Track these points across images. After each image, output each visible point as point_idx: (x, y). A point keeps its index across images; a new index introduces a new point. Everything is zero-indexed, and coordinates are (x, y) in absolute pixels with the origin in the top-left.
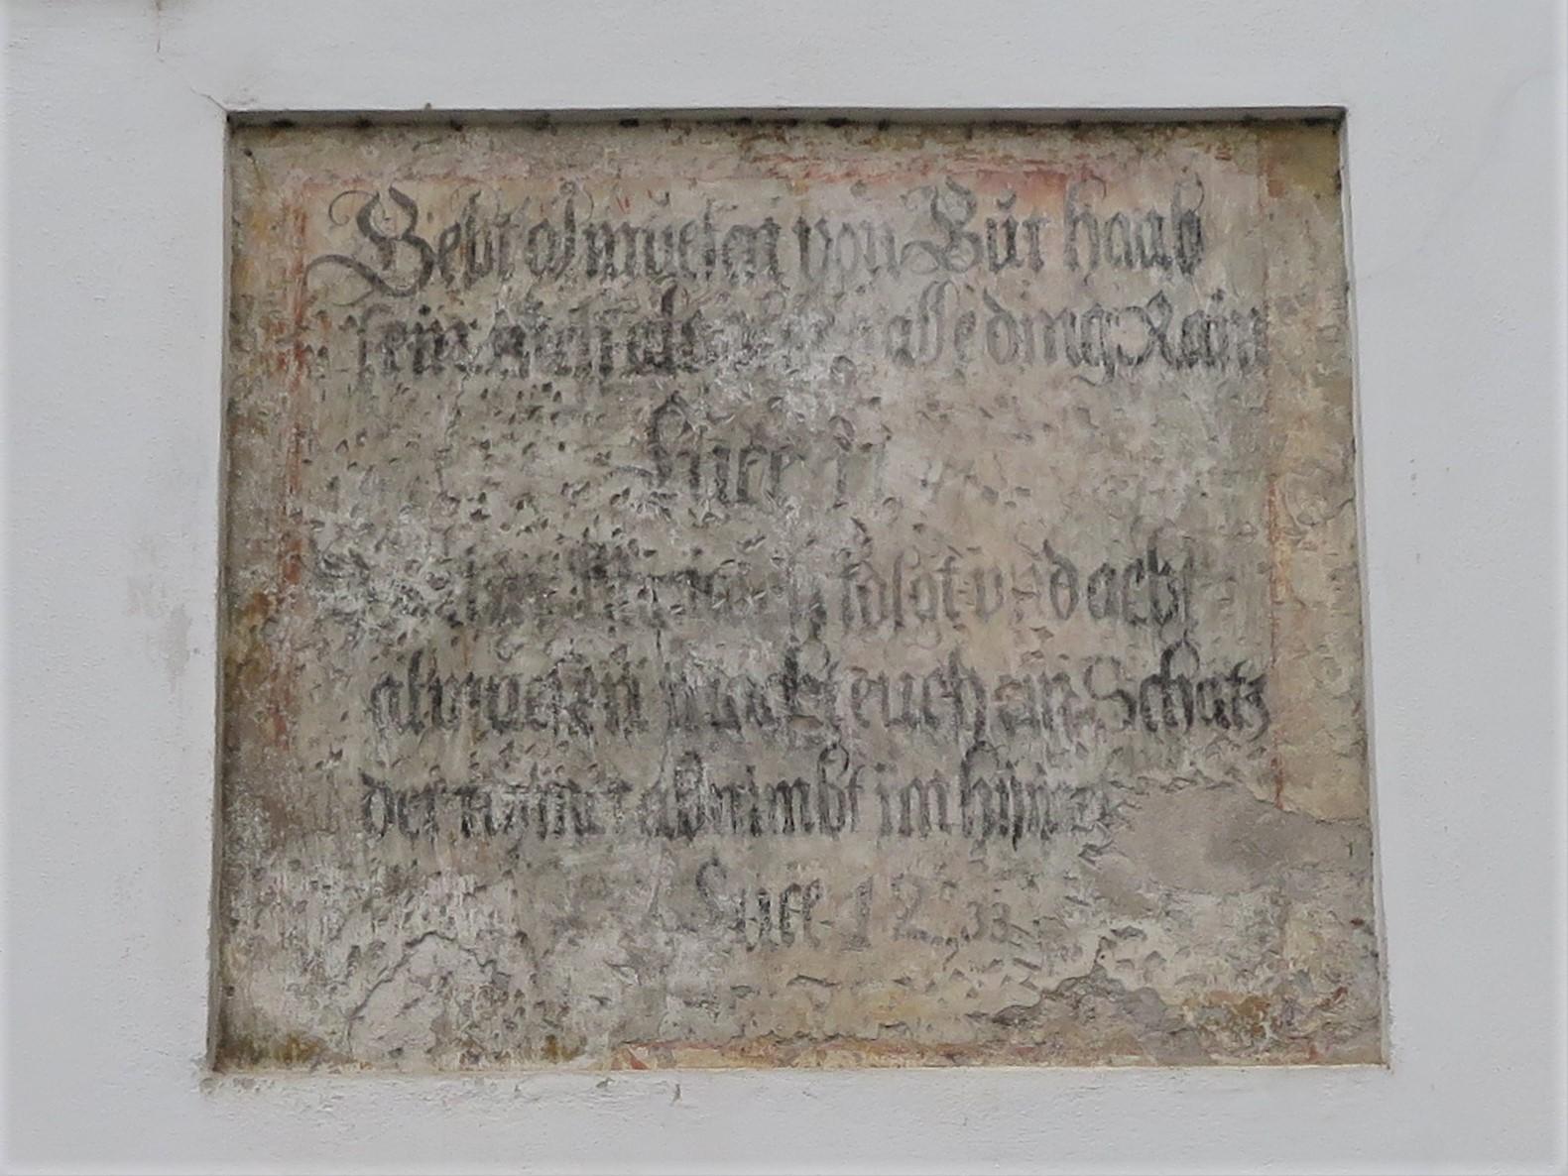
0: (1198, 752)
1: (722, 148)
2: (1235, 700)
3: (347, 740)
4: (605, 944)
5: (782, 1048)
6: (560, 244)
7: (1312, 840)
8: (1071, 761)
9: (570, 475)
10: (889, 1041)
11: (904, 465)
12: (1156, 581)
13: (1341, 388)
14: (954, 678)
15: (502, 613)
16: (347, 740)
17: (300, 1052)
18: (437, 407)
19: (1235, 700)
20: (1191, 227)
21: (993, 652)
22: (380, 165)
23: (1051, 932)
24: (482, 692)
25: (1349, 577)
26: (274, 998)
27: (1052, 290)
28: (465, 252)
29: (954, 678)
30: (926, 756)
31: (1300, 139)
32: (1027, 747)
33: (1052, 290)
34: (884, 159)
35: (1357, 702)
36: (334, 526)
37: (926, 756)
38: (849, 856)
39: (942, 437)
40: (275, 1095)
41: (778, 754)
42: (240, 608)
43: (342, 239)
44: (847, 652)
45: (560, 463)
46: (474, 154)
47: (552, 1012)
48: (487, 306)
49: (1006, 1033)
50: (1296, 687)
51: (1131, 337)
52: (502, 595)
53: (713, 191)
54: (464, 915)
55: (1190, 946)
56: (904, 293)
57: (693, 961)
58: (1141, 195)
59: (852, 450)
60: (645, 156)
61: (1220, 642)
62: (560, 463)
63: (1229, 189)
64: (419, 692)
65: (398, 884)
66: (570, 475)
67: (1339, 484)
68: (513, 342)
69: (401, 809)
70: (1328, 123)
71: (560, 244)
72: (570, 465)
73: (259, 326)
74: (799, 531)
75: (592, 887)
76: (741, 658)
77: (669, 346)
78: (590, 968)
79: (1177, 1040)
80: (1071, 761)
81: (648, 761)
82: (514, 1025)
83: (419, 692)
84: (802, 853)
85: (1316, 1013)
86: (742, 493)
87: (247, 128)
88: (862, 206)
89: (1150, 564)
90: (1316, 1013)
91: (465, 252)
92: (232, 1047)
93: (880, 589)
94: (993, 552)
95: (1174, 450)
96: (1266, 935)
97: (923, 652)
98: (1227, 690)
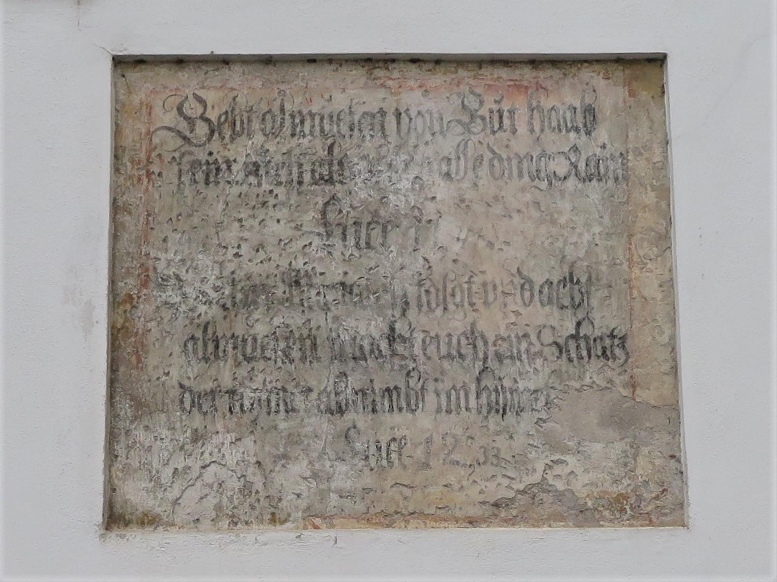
0: (594, 372)
1: (358, 73)
2: (612, 346)
3: (172, 366)
4: (300, 467)
5: (388, 518)
6: (277, 121)
7: (650, 416)
8: (531, 377)
9: (282, 235)
10: (441, 515)
11: (448, 230)
12: (573, 288)
13: (664, 192)
14: (473, 335)
15: (249, 304)
16: (172, 366)
17: (149, 521)
18: (216, 202)
19: (612, 346)
20: (590, 112)
21: (492, 322)
22: (188, 82)
23: (521, 461)
24: (239, 343)
25: (669, 286)
26: (136, 494)
27: (521, 144)
28: (230, 125)
29: (473, 335)
30: (459, 374)
31: (644, 69)
32: (509, 370)
33: (521, 144)
34: (438, 79)
35: (673, 347)
36: (166, 261)
37: (459, 374)
38: (420, 424)
39: (467, 216)
40: (136, 542)
41: (386, 373)
42: (119, 301)
43: (170, 118)
44: (420, 323)
45: (277, 229)
46: (235, 76)
47: (274, 501)
48: (241, 151)
49: (499, 511)
50: (642, 340)
51: (561, 167)
52: (249, 294)
53: (353, 95)
54: (230, 453)
55: (590, 468)
56: (448, 145)
57: (343, 476)
58: (566, 96)
59: (422, 223)
60: (319, 77)
61: (604, 318)
62: (277, 229)
63: (609, 94)
64: (208, 343)
65: (197, 437)
66: (282, 235)
67: (664, 239)
68: (254, 169)
69: (199, 400)
70: (658, 61)
71: (277, 121)
72: (283, 230)
73: (128, 161)
74: (396, 263)
75: (293, 439)
76: (367, 325)
77: (331, 171)
78: (292, 479)
79: (583, 515)
80: (531, 377)
81: (321, 377)
82: (255, 507)
83: (208, 343)
84: (397, 422)
85: (652, 502)
86: (368, 244)
87: (122, 63)
88: (427, 102)
89: (570, 279)
90: (652, 502)
91: (230, 125)
92: (115, 518)
93: (436, 292)
94: (492, 273)
95: (582, 223)
96: (627, 463)
97: (458, 323)
98: (608, 341)
